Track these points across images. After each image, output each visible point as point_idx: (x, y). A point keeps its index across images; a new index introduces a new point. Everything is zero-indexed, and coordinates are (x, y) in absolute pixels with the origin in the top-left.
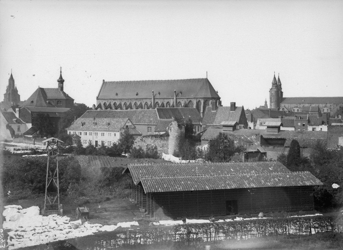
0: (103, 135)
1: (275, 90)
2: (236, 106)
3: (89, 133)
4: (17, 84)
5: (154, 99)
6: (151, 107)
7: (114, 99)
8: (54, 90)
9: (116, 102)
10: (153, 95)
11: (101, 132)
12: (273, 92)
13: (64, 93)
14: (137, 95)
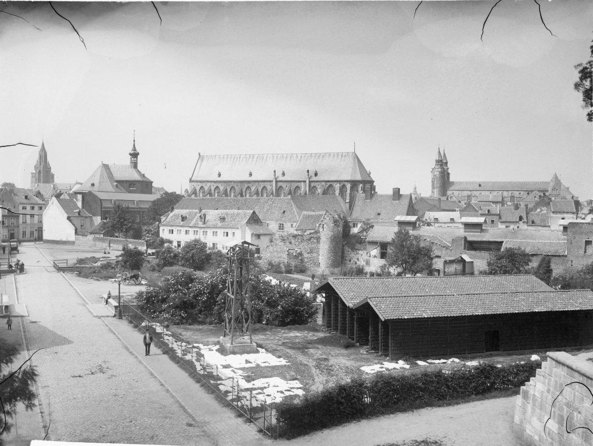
0: (215, 234)
1: (440, 170)
2: (401, 193)
3: (176, 230)
4: (50, 159)
5: (277, 182)
6: (272, 194)
7: (215, 182)
8: (124, 167)
9: (219, 185)
11: (223, 230)
12: (436, 173)
13: (139, 172)
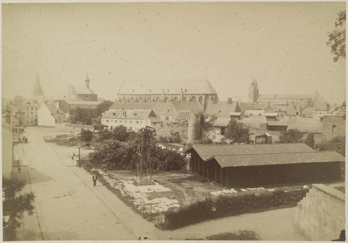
2: (232, 100)
5: (164, 95)
6: (162, 101)
7: (131, 95)
9: (134, 97)
10: (182, 91)
14: (150, 91)
